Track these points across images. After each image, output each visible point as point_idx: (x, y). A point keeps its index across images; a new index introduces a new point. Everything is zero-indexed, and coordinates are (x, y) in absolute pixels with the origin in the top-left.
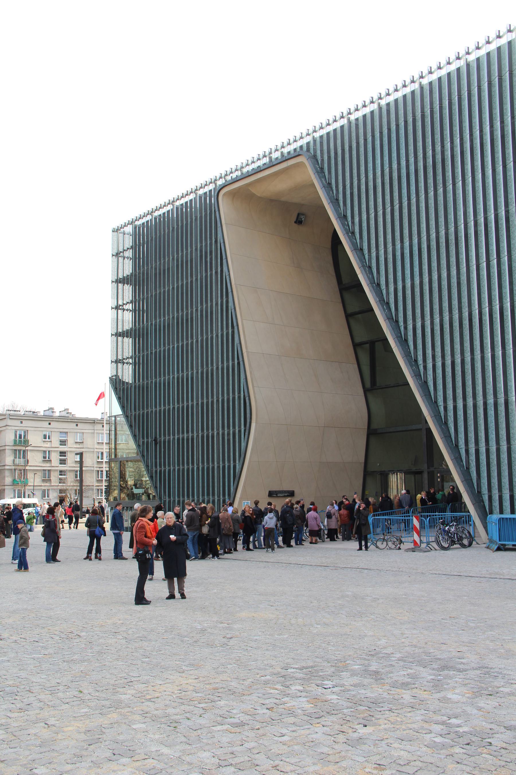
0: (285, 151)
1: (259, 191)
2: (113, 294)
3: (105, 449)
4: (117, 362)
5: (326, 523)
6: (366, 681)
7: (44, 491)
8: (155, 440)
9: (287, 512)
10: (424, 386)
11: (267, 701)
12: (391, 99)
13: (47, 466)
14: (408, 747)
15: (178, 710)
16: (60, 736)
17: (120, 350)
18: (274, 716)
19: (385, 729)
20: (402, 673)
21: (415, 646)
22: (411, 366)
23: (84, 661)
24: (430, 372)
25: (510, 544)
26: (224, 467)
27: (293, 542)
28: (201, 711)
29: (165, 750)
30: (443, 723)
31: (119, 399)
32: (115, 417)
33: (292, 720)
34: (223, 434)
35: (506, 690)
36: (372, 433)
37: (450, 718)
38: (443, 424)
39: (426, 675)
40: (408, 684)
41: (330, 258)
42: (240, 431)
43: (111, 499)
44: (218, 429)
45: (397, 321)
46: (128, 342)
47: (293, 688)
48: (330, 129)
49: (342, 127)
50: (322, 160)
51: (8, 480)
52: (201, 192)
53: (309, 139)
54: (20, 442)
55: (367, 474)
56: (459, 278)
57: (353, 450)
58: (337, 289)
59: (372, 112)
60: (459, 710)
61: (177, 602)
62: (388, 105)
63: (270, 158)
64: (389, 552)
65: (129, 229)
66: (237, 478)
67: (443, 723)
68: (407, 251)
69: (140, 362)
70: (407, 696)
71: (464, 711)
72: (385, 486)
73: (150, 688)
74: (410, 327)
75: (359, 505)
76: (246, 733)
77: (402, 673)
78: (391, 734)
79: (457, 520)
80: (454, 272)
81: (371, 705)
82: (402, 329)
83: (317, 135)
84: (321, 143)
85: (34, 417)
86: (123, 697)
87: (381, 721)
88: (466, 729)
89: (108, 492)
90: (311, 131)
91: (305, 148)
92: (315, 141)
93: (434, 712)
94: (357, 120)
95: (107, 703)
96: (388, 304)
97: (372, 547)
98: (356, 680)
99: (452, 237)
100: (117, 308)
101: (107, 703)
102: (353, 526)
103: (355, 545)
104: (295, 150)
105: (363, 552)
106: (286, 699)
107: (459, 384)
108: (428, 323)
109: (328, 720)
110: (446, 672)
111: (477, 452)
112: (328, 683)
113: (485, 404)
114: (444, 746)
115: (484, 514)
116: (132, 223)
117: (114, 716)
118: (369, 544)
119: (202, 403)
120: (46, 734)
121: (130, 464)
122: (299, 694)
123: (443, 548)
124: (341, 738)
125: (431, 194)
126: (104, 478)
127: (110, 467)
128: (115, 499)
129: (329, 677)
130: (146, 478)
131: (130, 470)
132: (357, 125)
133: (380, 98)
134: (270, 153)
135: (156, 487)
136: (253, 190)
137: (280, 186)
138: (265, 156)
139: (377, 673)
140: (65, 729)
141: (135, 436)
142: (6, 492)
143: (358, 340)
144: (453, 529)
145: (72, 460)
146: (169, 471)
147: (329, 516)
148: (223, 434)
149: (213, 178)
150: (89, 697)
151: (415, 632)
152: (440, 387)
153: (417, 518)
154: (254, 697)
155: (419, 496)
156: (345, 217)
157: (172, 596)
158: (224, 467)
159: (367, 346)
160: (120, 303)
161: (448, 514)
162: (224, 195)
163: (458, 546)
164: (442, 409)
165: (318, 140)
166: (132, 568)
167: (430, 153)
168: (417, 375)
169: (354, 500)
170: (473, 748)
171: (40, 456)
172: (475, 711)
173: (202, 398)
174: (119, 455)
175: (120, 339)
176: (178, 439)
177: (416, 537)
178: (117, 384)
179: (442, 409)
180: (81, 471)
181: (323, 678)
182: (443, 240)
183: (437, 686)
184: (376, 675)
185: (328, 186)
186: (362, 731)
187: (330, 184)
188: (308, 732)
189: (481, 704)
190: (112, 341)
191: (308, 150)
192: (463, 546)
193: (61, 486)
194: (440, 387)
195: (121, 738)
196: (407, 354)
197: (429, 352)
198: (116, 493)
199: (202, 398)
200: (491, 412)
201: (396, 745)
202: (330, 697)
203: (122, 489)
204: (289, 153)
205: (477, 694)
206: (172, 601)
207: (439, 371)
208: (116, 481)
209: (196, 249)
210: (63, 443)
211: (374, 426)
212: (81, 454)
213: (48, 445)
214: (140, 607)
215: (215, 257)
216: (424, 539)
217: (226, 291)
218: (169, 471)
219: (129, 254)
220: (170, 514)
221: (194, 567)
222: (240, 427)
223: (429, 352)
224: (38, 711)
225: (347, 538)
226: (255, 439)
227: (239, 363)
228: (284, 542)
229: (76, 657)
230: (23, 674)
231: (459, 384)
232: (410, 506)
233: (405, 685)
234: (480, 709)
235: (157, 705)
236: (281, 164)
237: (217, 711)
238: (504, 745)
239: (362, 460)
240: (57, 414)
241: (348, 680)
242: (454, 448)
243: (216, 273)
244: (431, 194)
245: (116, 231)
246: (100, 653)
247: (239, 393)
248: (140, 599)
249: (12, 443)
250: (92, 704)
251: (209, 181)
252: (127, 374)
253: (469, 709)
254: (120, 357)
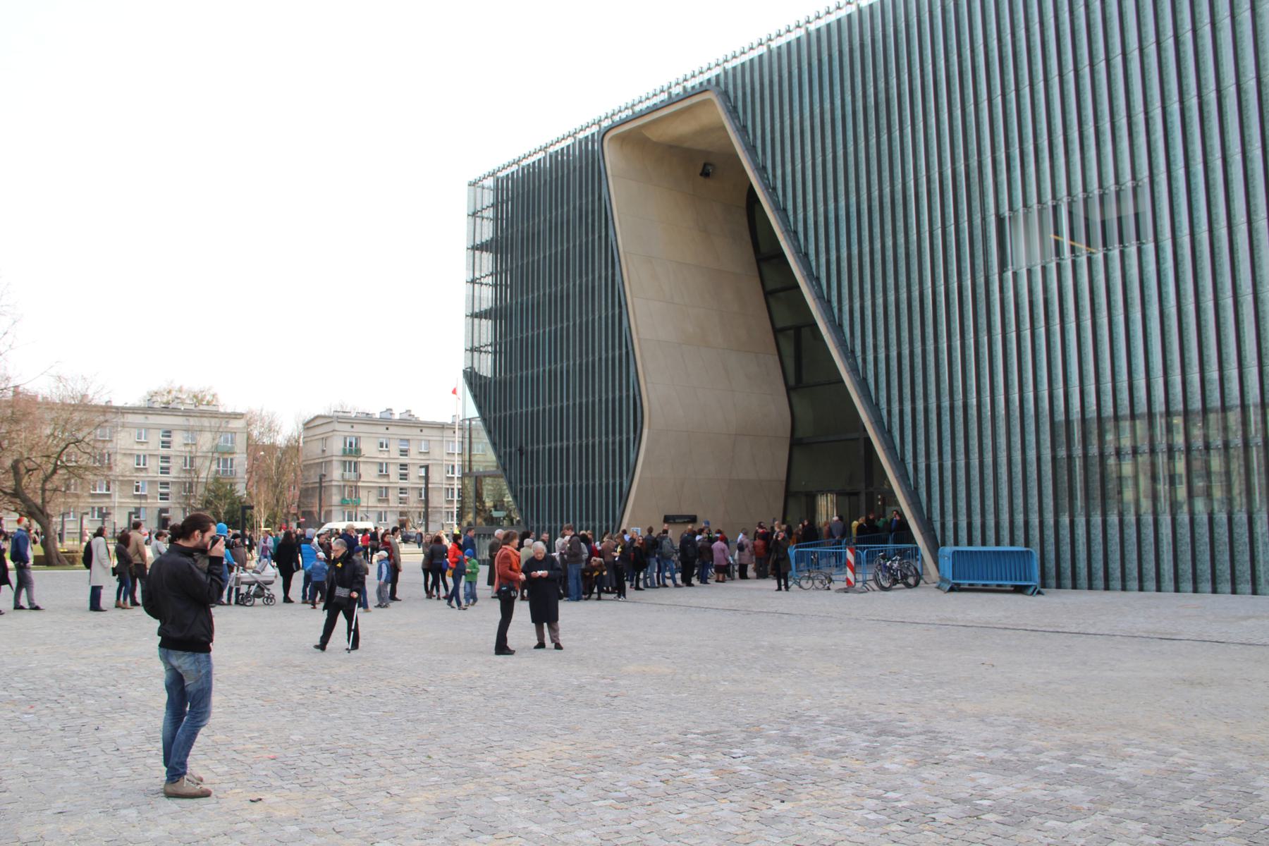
0: (689, 85)
1: (655, 135)
2: (468, 264)
3: (457, 461)
4: (472, 350)
5: (736, 556)
6: (785, 749)
7: (380, 514)
8: (521, 450)
9: (689, 542)
10: (862, 383)
11: (661, 773)
12: (822, 23)
13: (383, 482)
14: (835, 826)
15: (550, 782)
16: (405, 808)
17: (476, 335)
18: (670, 789)
19: (807, 805)
20: (830, 739)
21: (847, 708)
22: (847, 358)
23: (433, 721)
24: (871, 366)
25: (965, 583)
26: (607, 485)
27: (694, 581)
28: (579, 783)
29: (535, 828)
30: (878, 797)
31: (475, 397)
32: (470, 420)
33: (692, 794)
34: (607, 443)
35: (957, 757)
36: (796, 443)
37: (887, 791)
38: (886, 433)
39: (860, 741)
40: (836, 752)
41: (745, 221)
42: (628, 439)
43: (465, 524)
44: (600, 437)
45: (829, 301)
46: (487, 325)
47: (694, 757)
48: (745, 58)
49: (761, 57)
50: (736, 97)
51: (336, 499)
52: (581, 135)
53: (718, 70)
54: (351, 451)
55: (789, 494)
56: (907, 248)
57: (772, 465)
58: (753, 260)
59: (798, 39)
60: (899, 782)
61: (549, 652)
62: (818, 30)
63: (670, 94)
64: (816, 593)
65: (490, 182)
66: (624, 498)
67: (878, 797)
68: (842, 213)
69: (503, 348)
70: (834, 767)
71: (904, 783)
72: (812, 511)
73: (515, 755)
74: (846, 308)
75: (779, 533)
76: (635, 810)
77: (830, 739)
78: (814, 810)
79: (902, 553)
80: (901, 240)
81: (791, 777)
82: (836, 310)
83: (729, 66)
84: (734, 76)
85: (367, 420)
86: (482, 765)
87: (803, 796)
88: (905, 803)
89: (461, 516)
90: (721, 61)
91: (714, 82)
92: (726, 72)
93: (868, 785)
94: (779, 48)
95: (462, 771)
96: (818, 279)
97: (794, 587)
98: (772, 747)
99: (899, 197)
100: (473, 281)
101: (462, 771)
102: (772, 562)
103: (772, 584)
104: (701, 84)
105: (783, 593)
106: (684, 770)
107: (907, 382)
108: (868, 303)
109: (737, 795)
110: (884, 738)
111: (928, 467)
112: (737, 752)
113: (939, 407)
114: (878, 823)
115: (934, 547)
116: (493, 174)
117: (472, 787)
118: (790, 583)
119: (581, 404)
120: (388, 804)
121: (488, 480)
122: (701, 764)
123: (883, 589)
124: (753, 816)
125: (873, 141)
126: (456, 498)
127: (463, 484)
128: (469, 524)
129: (739, 744)
130: (508, 498)
131: (488, 487)
132: (779, 55)
133: (808, 22)
134: (670, 87)
135: (521, 510)
136: (648, 134)
137: (682, 128)
138: (662, 91)
139: (798, 739)
140: (412, 800)
141: (494, 444)
142: (334, 513)
143: (779, 325)
144: (895, 565)
145: (415, 474)
146: (538, 488)
147: (741, 548)
148: (607, 443)
149: (572, 131)
150: (440, 763)
151: (846, 690)
152: (883, 385)
153: (851, 550)
154: (644, 767)
155: (855, 523)
156: (764, 168)
157: (541, 645)
158: (607, 485)
159: (791, 332)
160: (477, 275)
161: (891, 546)
162: (611, 139)
163: (901, 585)
164: (884, 413)
165: (730, 73)
166: (493, 611)
167: (871, 91)
168: (853, 369)
169: (772, 528)
170: (913, 824)
171: (375, 469)
172: (918, 783)
173: (581, 397)
174: (474, 469)
175: (476, 321)
176: (550, 449)
177: (850, 574)
178: (472, 378)
179: (884, 413)
180: (427, 489)
181: (731, 746)
182: (887, 200)
183: (873, 754)
184: (798, 742)
185: (742, 130)
186: (779, 807)
187: (745, 127)
188: (711, 808)
189: (925, 775)
190: (466, 325)
191: (718, 83)
192: (908, 586)
193: (401, 507)
194: (883, 385)
195: (480, 812)
196: (841, 343)
197: (870, 340)
198: (470, 517)
199: (581, 397)
200: (946, 418)
201: (820, 823)
202: (739, 768)
203: (477, 512)
204: (693, 88)
205: (920, 763)
206: (541, 651)
207: (882, 366)
208: (470, 502)
209: (574, 208)
210: (404, 453)
211: (799, 434)
212: (427, 467)
213: (386, 455)
214: (501, 658)
215: (597, 217)
216: (860, 577)
217: (612, 261)
218: (538, 488)
219: (489, 213)
220: (540, 544)
221: (568, 611)
222: (628, 433)
223: (870, 340)
224: (378, 778)
225: (762, 575)
226: (647, 450)
227: (627, 353)
228: (683, 579)
229: (422, 716)
230: (358, 734)
231: (907, 382)
232: (843, 536)
233: (833, 754)
234: (923, 780)
235: (524, 775)
236: (685, 101)
237: (599, 784)
238: (951, 821)
239: (783, 477)
240: (397, 417)
241: (762, 747)
242: (899, 464)
243: (600, 237)
244: (873, 141)
245: (473, 184)
246: (452, 712)
247: (628, 390)
248: (502, 648)
249: (341, 453)
250: (444, 772)
251: (591, 121)
252: (485, 366)
253: (911, 781)
254: (476, 344)
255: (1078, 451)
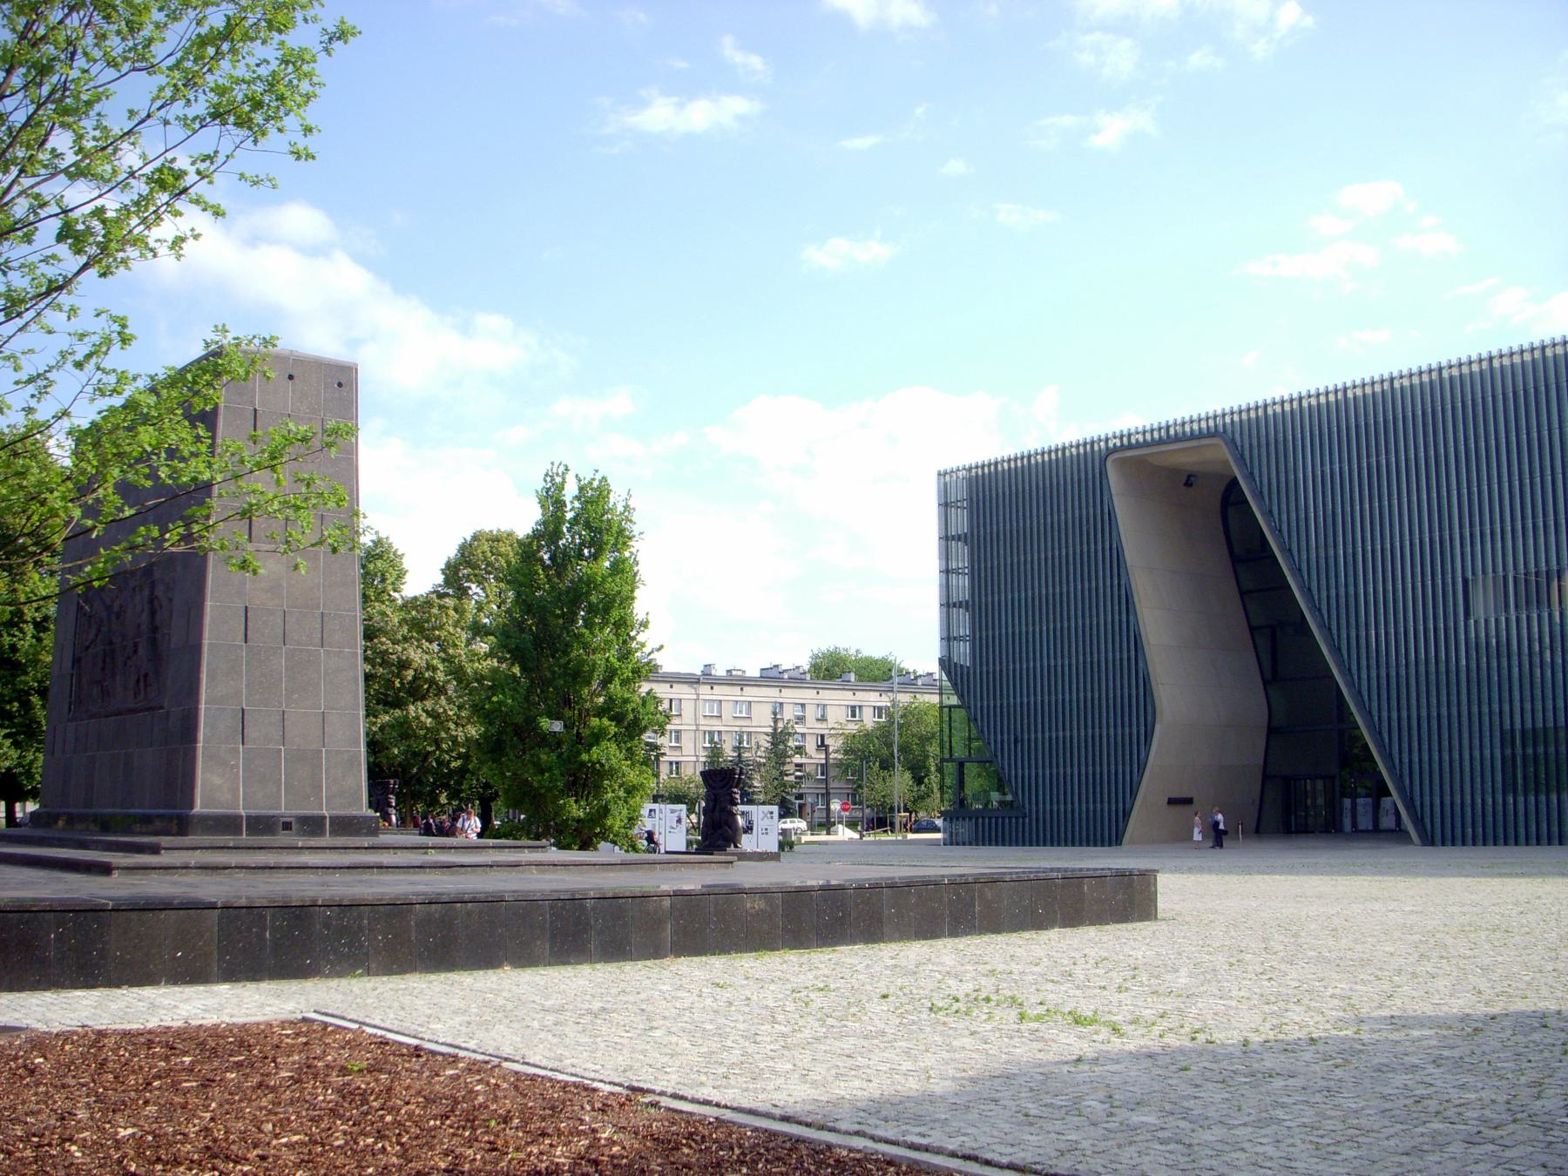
36: (1272, 731)
111: (1410, 761)
168: (1350, 685)
255: (1519, 750)
